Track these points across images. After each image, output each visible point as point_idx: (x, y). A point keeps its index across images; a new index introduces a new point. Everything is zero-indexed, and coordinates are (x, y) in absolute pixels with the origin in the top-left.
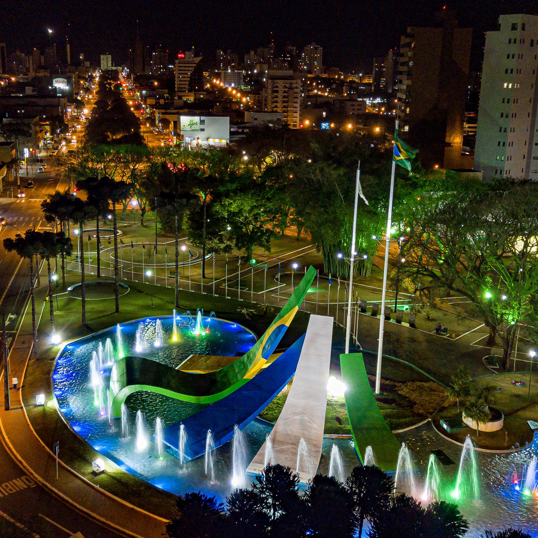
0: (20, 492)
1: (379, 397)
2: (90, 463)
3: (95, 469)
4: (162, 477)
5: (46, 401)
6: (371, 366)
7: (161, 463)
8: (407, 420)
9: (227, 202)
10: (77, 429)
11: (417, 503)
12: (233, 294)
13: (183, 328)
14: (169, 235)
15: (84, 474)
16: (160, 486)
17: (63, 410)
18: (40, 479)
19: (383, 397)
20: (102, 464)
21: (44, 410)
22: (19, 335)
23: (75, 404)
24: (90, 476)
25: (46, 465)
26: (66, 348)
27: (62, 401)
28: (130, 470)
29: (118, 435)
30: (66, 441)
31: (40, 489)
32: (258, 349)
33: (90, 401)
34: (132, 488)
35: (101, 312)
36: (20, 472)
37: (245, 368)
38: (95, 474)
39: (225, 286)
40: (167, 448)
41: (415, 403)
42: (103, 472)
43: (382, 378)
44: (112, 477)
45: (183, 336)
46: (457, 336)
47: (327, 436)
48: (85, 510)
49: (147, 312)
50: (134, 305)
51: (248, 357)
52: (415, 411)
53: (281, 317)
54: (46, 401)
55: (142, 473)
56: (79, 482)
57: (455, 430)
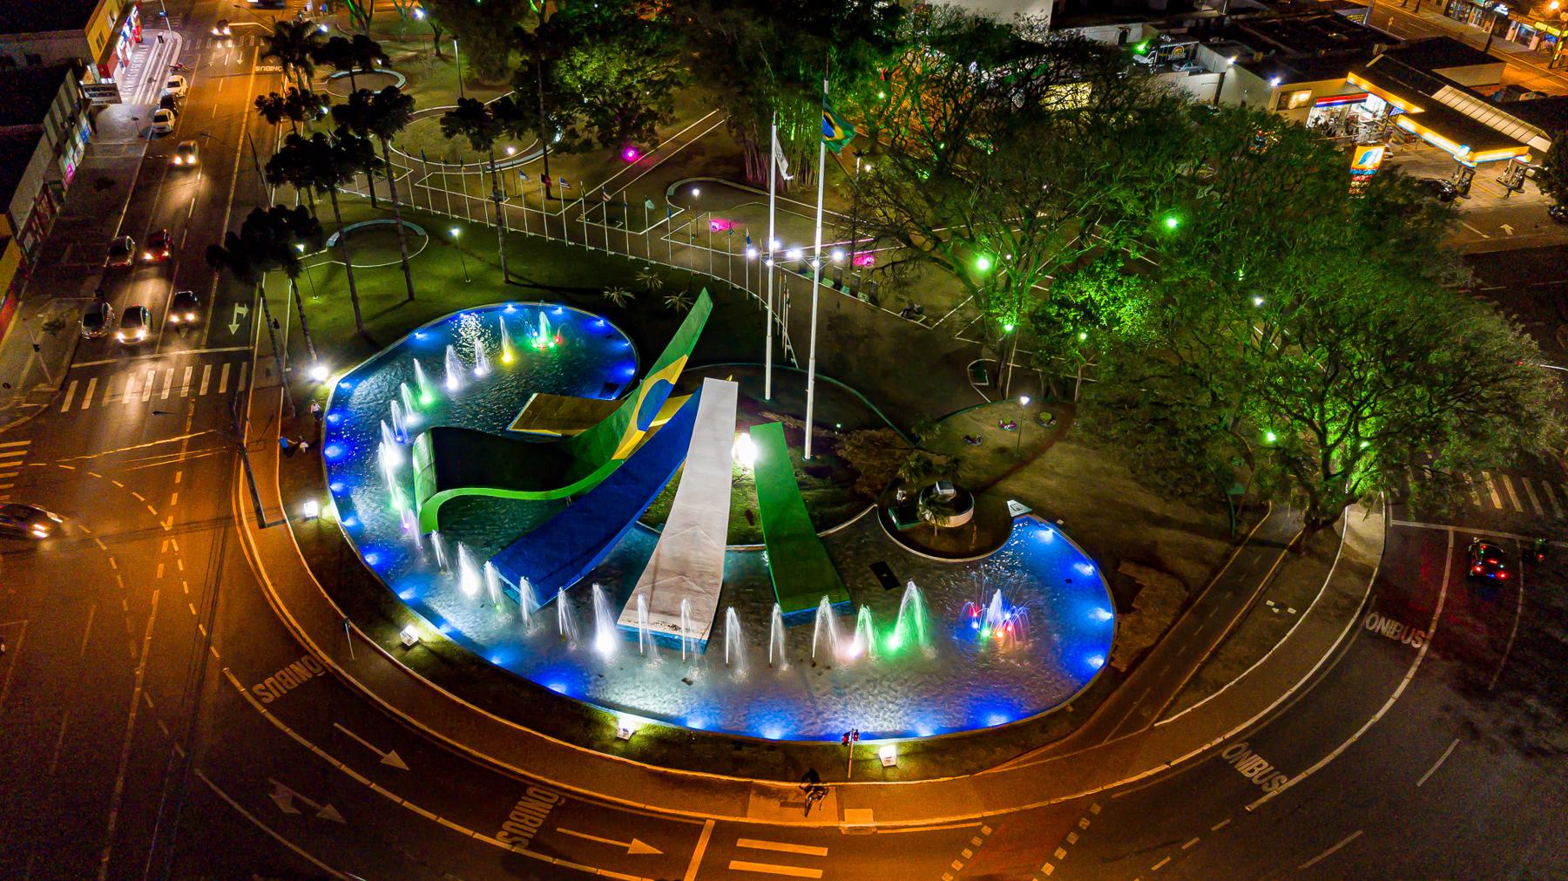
0: (304, 686)
1: (811, 465)
2: (399, 628)
3: (405, 640)
4: (499, 644)
5: (319, 510)
6: (760, 621)
7: (500, 617)
8: (844, 508)
9: (580, 57)
10: (371, 559)
11: (864, 613)
12: (596, 238)
13: (517, 330)
14: (487, 83)
15: (390, 649)
16: (495, 661)
17: (349, 523)
18: (329, 660)
19: (817, 464)
20: (417, 631)
21: (319, 527)
22: (259, 357)
23: (365, 511)
24: (400, 651)
25: (333, 639)
26: (338, 387)
27: (345, 507)
28: (456, 635)
29: (434, 568)
30: (357, 584)
31: (331, 680)
32: (632, 408)
33: (384, 501)
34: (459, 665)
35: (387, 297)
36: (299, 651)
37: (613, 443)
38: (405, 647)
39: (583, 219)
40: (505, 587)
41: (859, 474)
42: (417, 643)
43: (815, 424)
44: (431, 652)
45: (520, 350)
46: (937, 319)
47: (733, 547)
48: (398, 712)
49: (460, 298)
50: (437, 278)
51: (619, 421)
52: (858, 488)
53: (665, 365)
54: (319, 510)
55: (475, 637)
56: (384, 662)
57: (907, 527)
